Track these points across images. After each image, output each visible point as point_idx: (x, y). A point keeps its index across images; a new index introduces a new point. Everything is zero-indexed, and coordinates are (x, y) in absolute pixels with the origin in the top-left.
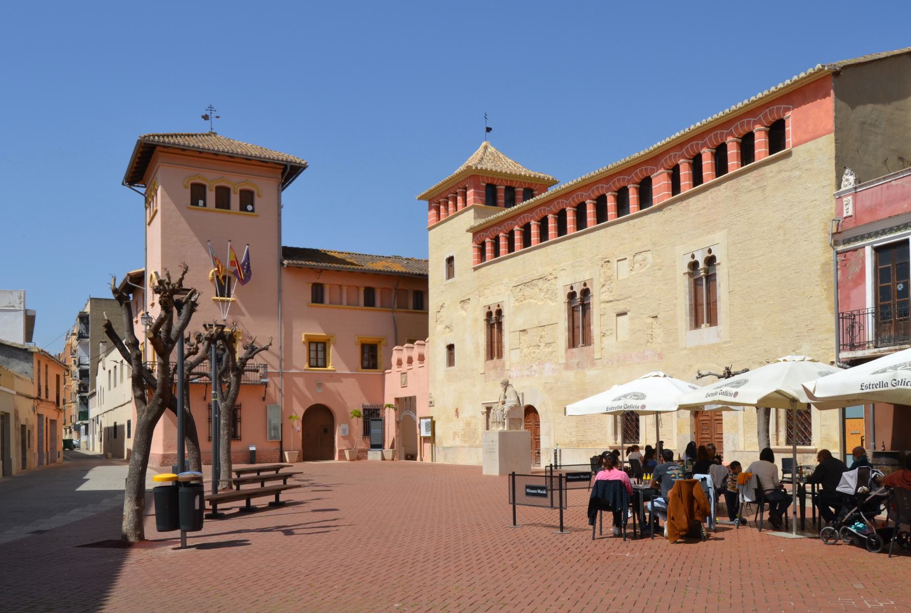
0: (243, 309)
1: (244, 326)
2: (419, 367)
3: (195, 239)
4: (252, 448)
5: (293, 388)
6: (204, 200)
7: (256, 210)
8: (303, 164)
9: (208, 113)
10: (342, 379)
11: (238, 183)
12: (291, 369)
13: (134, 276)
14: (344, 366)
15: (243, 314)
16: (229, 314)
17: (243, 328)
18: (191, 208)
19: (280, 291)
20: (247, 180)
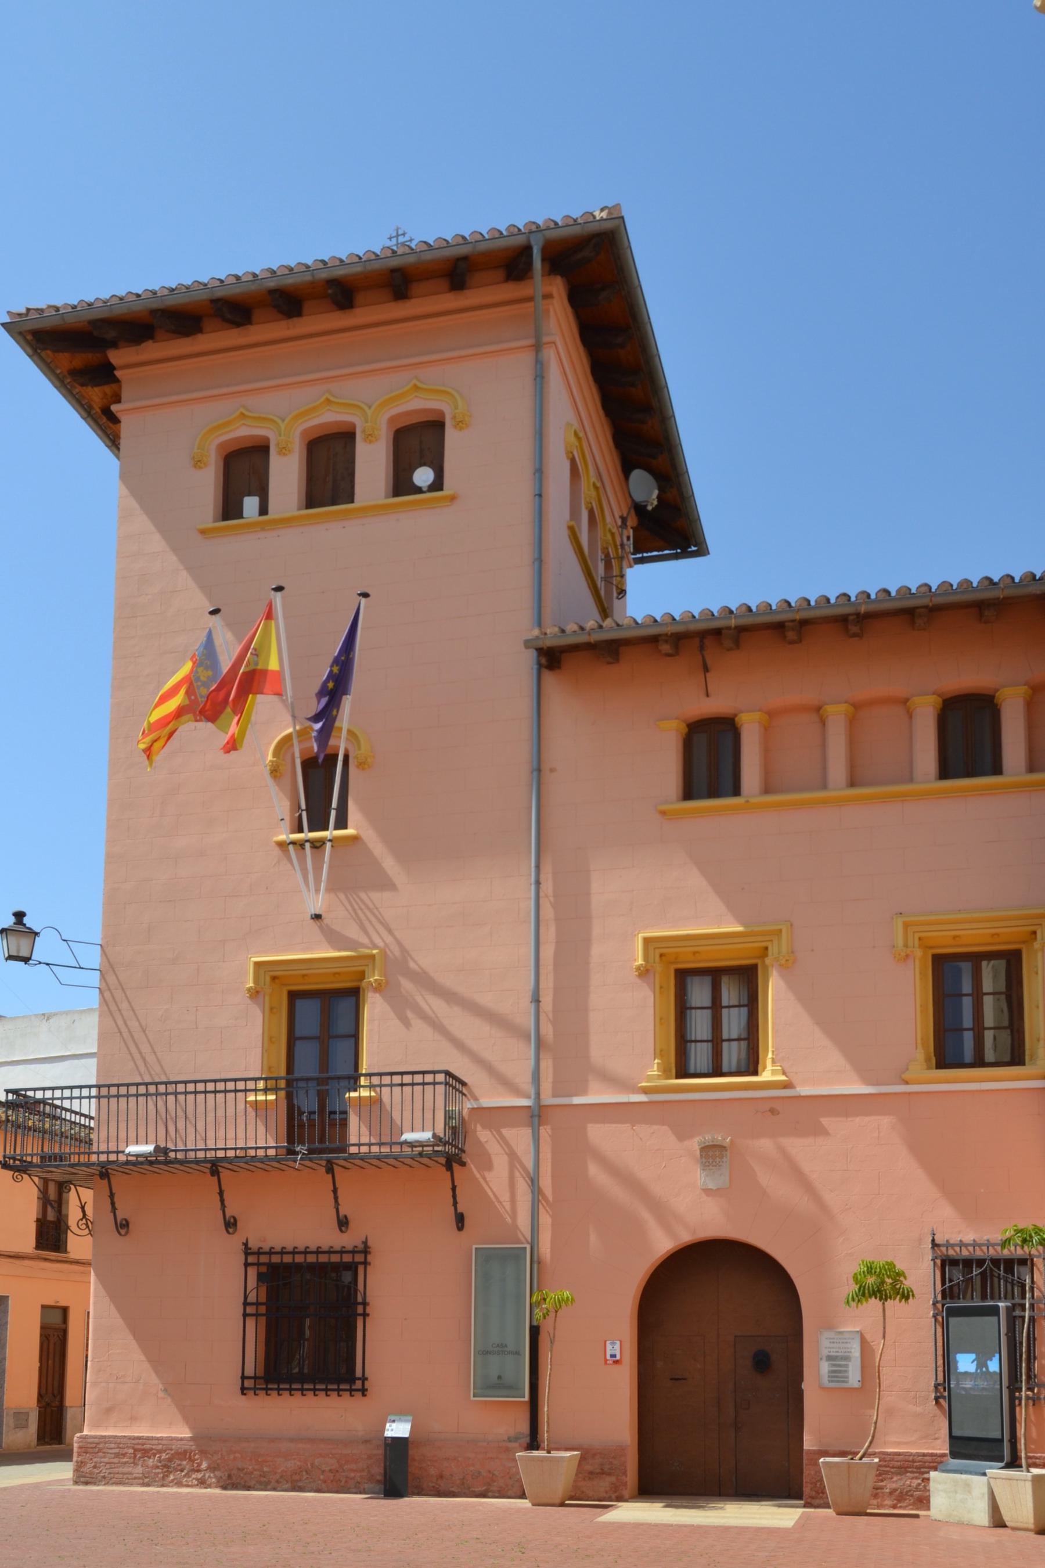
1: (390, 931)
4: (398, 1429)
5: (593, 1170)
6: (263, 493)
10: (825, 1121)
12: (584, 1092)
14: (836, 1059)
16: (328, 890)
17: (389, 939)
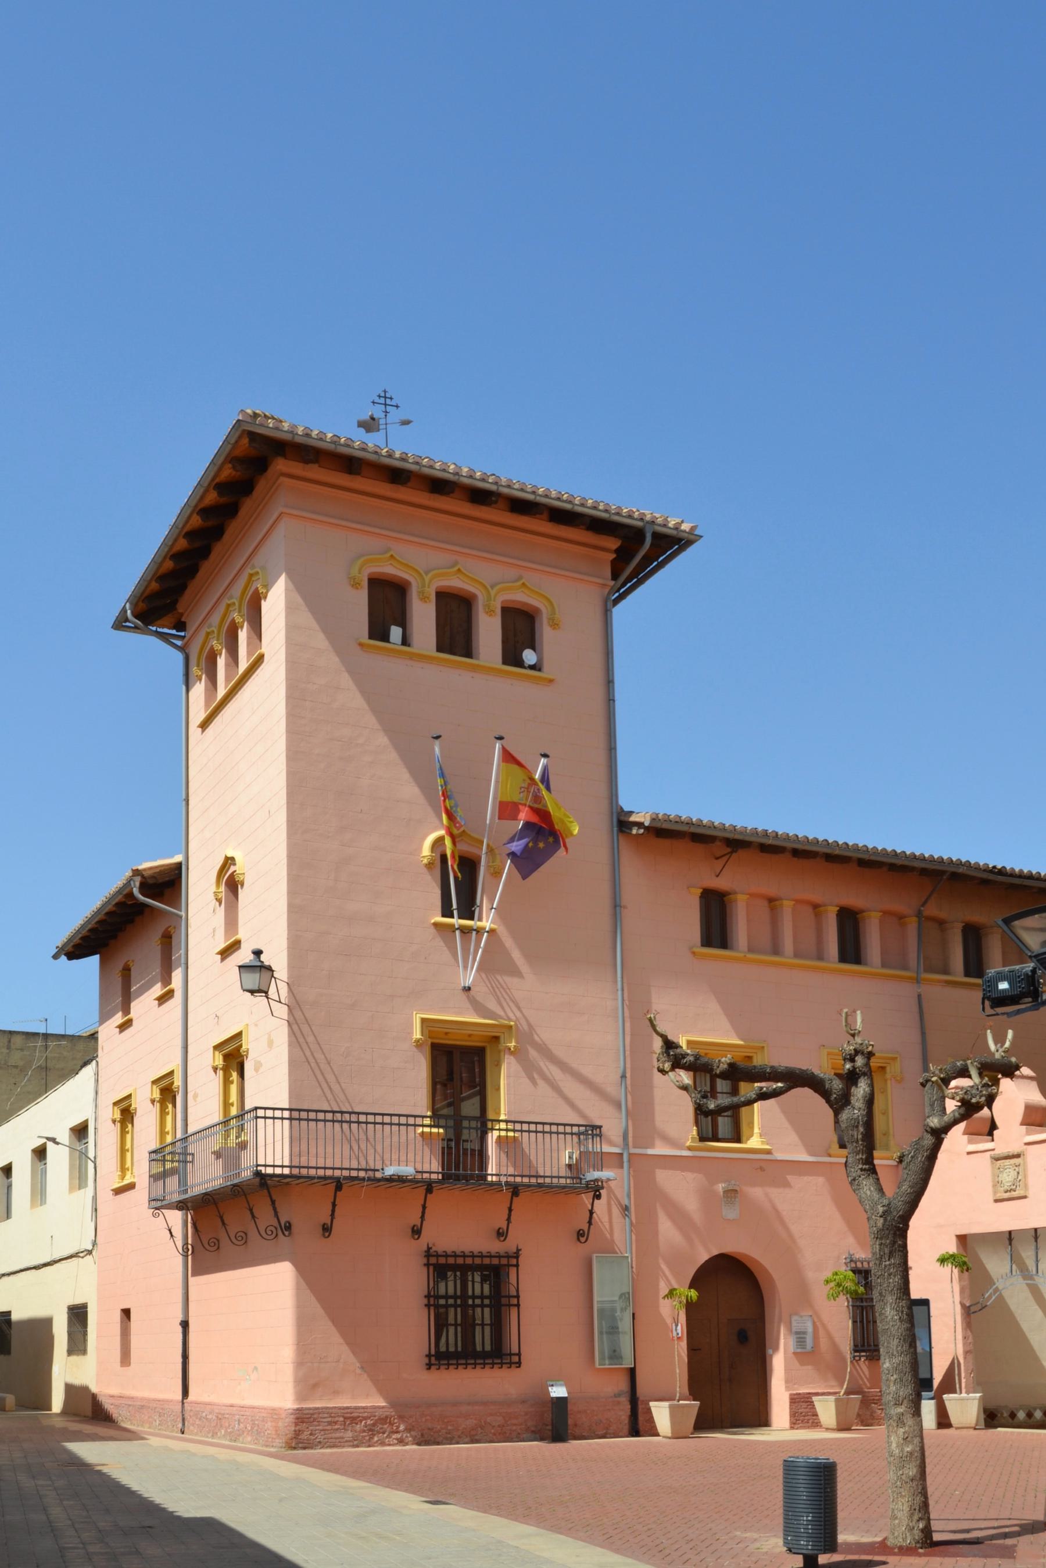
0: (516, 955)
2: (969, 1153)
3: (383, 740)
4: (558, 1391)
7: (546, 666)
8: (685, 531)
9: (378, 412)
10: (789, 1178)
11: (496, 584)
13: (153, 877)
14: (793, 1137)
15: (516, 972)
16: (479, 969)
17: (518, 1014)
18: (369, 646)
19: (616, 906)
20: (520, 578)
